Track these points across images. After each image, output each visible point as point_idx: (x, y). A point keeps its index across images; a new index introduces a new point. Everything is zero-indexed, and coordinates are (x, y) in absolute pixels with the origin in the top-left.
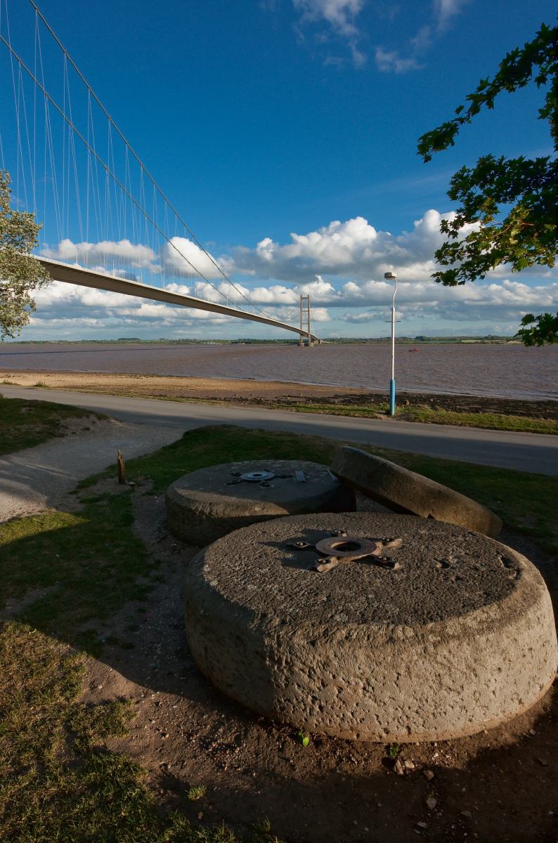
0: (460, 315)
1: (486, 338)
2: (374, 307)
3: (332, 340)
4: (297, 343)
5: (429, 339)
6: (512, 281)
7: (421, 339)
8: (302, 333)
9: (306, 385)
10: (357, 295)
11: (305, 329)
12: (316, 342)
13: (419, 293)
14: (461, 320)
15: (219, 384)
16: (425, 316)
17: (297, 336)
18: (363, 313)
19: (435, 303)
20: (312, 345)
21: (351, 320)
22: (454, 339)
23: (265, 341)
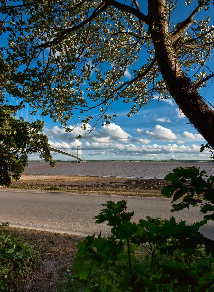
0: (121, 154)
1: (131, 160)
2: (96, 151)
3: (87, 161)
4: (76, 162)
5: (116, 161)
6: (131, 144)
7: (113, 160)
8: (78, 158)
9: (103, 177)
10: (89, 146)
11: (79, 157)
12: (82, 162)
13: (107, 146)
14: (122, 155)
15: (68, 178)
16: (111, 154)
17: (75, 159)
18: (93, 152)
19: (113, 150)
20: (81, 162)
21: (90, 154)
22: (123, 161)
23: (34, 161)
